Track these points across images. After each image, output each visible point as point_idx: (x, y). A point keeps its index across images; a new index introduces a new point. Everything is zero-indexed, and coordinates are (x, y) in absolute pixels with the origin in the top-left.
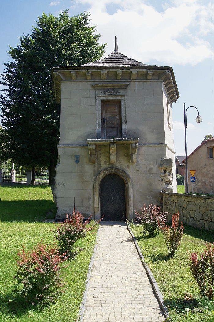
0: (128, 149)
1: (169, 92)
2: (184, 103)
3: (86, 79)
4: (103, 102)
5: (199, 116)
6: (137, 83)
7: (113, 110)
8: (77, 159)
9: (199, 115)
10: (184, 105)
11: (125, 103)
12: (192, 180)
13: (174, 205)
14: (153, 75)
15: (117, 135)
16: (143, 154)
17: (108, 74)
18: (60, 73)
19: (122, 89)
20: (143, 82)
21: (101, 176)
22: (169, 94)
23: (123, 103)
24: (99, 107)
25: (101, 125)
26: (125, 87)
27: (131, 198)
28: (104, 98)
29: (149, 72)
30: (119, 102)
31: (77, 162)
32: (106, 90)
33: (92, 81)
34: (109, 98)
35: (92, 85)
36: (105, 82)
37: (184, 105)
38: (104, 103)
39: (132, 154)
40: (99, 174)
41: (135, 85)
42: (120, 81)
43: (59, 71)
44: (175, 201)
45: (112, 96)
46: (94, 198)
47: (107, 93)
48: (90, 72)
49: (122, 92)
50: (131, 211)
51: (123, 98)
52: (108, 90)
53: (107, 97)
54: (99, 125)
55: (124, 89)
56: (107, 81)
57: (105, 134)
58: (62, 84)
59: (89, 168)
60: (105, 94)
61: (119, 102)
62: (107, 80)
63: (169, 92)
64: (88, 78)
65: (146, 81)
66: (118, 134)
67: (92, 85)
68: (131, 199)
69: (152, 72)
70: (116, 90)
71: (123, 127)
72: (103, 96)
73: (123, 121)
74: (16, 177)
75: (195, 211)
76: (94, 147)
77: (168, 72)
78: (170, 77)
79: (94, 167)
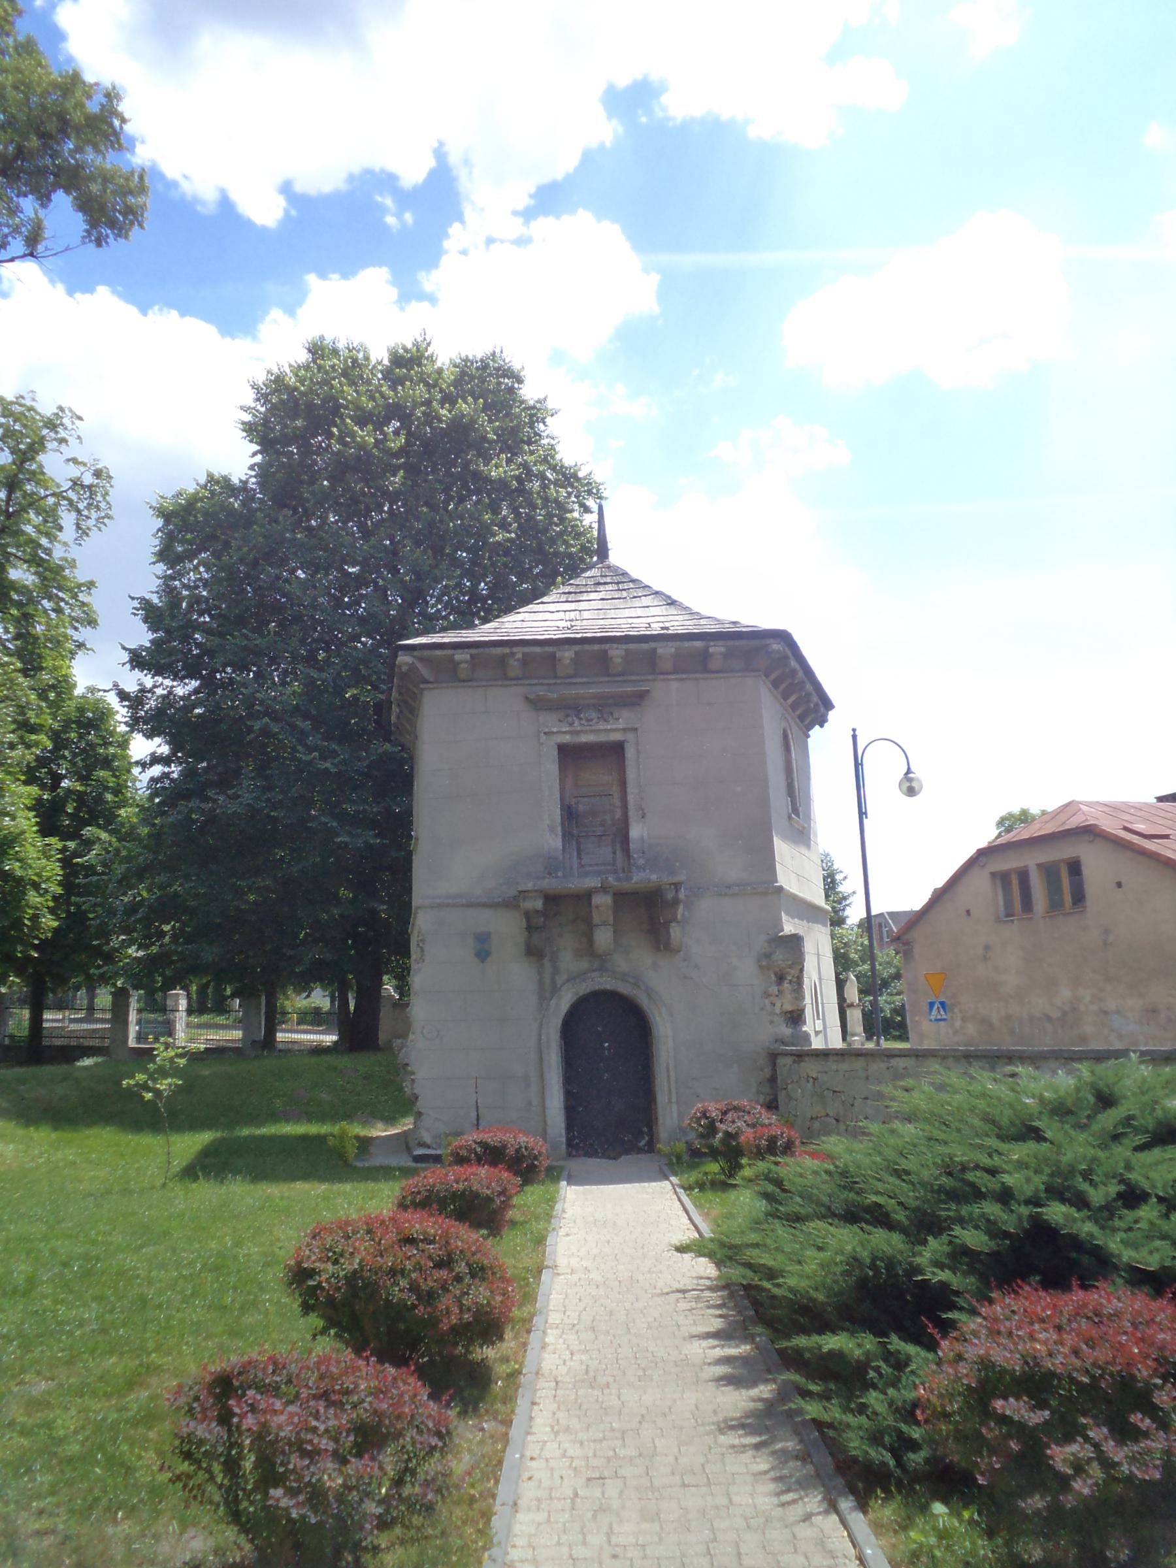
0: (651, 911)
1: (790, 701)
2: (854, 730)
3: (507, 678)
4: (563, 749)
5: (909, 771)
6: (674, 685)
7: (599, 776)
8: (483, 949)
9: (909, 768)
10: (854, 737)
11: (638, 752)
12: (934, 1012)
13: (810, 1085)
14: (726, 656)
15: (614, 859)
16: (702, 929)
17: (576, 661)
18: (421, 659)
19: (625, 705)
20: (696, 679)
21: (565, 1002)
22: (794, 707)
23: (630, 752)
24: (551, 766)
25: (559, 828)
26: (637, 700)
27: (668, 1070)
28: (567, 739)
29: (711, 650)
30: (616, 750)
31: (483, 954)
32: (571, 708)
33: (527, 682)
34: (584, 739)
35: (527, 698)
36: (570, 684)
37: (854, 737)
38: (569, 754)
39: (667, 924)
40: (555, 990)
41: (669, 692)
42: (616, 679)
43: (416, 653)
44: (811, 1074)
45: (592, 731)
46: (542, 1077)
47: (576, 723)
48: (519, 656)
49: (625, 718)
50: (673, 1115)
51: (630, 737)
52: (580, 711)
53: (578, 733)
54: (552, 829)
55: (633, 704)
56: (574, 680)
57: (575, 860)
58: (426, 693)
59: (518, 973)
60: (571, 724)
61: (616, 750)
62: (575, 676)
63: (790, 701)
64: (511, 674)
65: (706, 675)
66: (619, 854)
67: (527, 698)
68: (669, 1076)
69: (723, 649)
70: (605, 707)
71: (636, 832)
72: (565, 732)
73: (632, 813)
74: (188, 1025)
75: (866, 1098)
76: (539, 904)
77: (776, 646)
78: (787, 658)
79: (540, 973)
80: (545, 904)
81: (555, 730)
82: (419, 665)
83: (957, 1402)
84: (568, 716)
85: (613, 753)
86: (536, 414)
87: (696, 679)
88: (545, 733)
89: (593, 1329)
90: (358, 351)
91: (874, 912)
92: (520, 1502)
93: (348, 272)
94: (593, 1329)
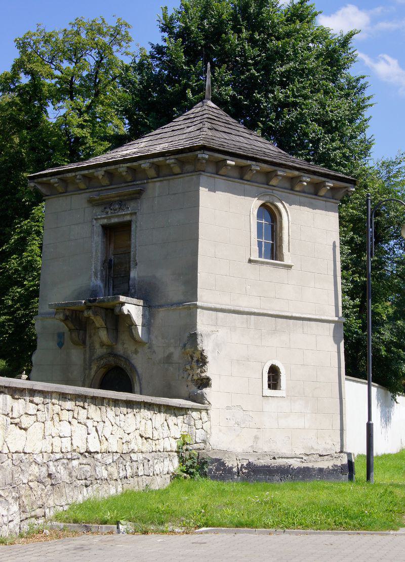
6: (158, 184)
20: (169, 180)
24: (98, 240)
28: (105, 221)
32: (106, 204)
38: (109, 231)
41: (155, 189)
43: (36, 181)
53: (109, 218)
55: (136, 199)
70: (122, 202)
72: (104, 218)
80: (86, 317)
81: (99, 217)
82: (39, 187)
83: (294, 141)
84: (105, 208)
85: (125, 228)
86: (384, 454)
87: (169, 180)
88: (95, 219)
89: (102, 480)
90: (78, 33)
91: (199, 310)
92: (371, 99)
93: (258, 247)
94: (102, 480)
